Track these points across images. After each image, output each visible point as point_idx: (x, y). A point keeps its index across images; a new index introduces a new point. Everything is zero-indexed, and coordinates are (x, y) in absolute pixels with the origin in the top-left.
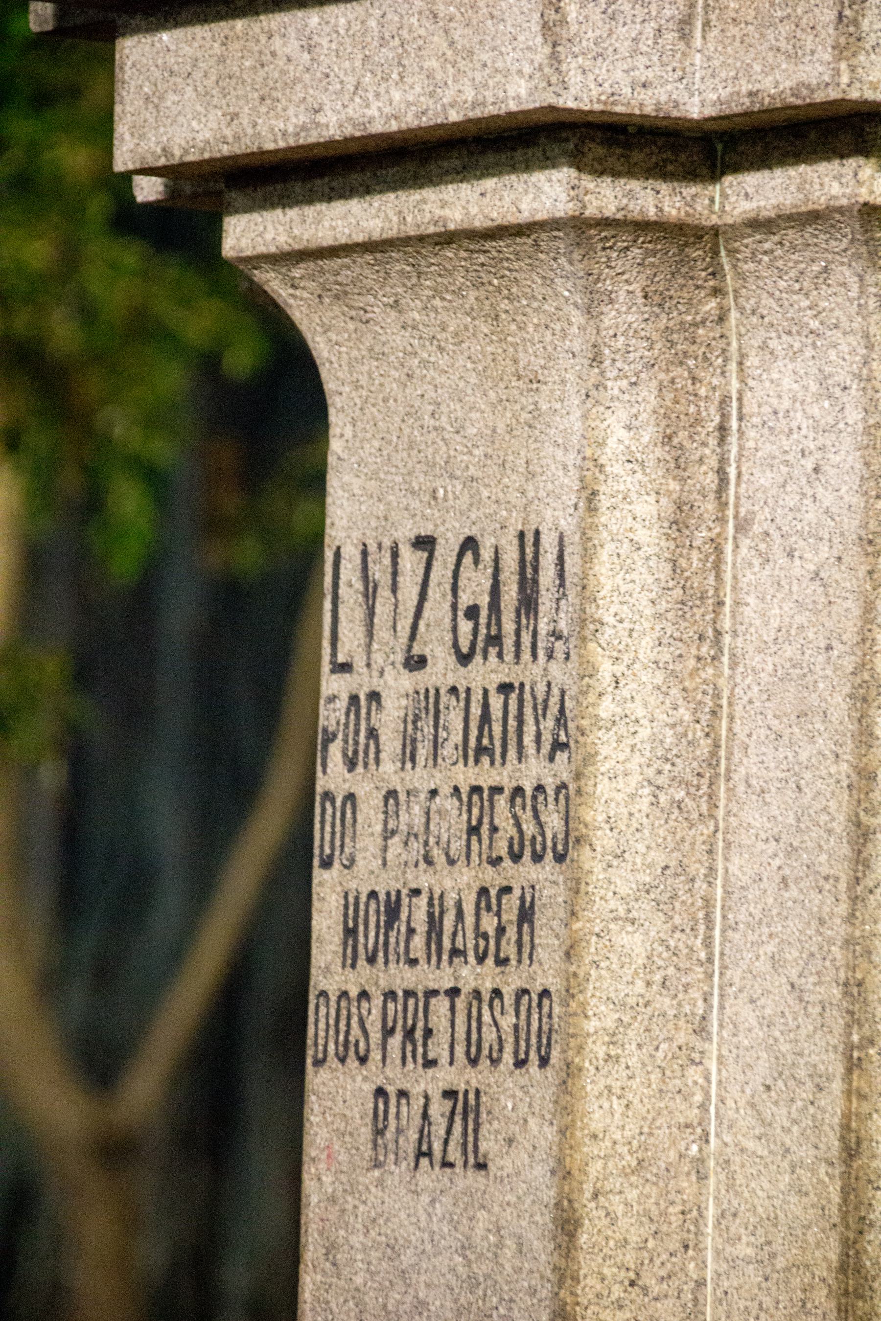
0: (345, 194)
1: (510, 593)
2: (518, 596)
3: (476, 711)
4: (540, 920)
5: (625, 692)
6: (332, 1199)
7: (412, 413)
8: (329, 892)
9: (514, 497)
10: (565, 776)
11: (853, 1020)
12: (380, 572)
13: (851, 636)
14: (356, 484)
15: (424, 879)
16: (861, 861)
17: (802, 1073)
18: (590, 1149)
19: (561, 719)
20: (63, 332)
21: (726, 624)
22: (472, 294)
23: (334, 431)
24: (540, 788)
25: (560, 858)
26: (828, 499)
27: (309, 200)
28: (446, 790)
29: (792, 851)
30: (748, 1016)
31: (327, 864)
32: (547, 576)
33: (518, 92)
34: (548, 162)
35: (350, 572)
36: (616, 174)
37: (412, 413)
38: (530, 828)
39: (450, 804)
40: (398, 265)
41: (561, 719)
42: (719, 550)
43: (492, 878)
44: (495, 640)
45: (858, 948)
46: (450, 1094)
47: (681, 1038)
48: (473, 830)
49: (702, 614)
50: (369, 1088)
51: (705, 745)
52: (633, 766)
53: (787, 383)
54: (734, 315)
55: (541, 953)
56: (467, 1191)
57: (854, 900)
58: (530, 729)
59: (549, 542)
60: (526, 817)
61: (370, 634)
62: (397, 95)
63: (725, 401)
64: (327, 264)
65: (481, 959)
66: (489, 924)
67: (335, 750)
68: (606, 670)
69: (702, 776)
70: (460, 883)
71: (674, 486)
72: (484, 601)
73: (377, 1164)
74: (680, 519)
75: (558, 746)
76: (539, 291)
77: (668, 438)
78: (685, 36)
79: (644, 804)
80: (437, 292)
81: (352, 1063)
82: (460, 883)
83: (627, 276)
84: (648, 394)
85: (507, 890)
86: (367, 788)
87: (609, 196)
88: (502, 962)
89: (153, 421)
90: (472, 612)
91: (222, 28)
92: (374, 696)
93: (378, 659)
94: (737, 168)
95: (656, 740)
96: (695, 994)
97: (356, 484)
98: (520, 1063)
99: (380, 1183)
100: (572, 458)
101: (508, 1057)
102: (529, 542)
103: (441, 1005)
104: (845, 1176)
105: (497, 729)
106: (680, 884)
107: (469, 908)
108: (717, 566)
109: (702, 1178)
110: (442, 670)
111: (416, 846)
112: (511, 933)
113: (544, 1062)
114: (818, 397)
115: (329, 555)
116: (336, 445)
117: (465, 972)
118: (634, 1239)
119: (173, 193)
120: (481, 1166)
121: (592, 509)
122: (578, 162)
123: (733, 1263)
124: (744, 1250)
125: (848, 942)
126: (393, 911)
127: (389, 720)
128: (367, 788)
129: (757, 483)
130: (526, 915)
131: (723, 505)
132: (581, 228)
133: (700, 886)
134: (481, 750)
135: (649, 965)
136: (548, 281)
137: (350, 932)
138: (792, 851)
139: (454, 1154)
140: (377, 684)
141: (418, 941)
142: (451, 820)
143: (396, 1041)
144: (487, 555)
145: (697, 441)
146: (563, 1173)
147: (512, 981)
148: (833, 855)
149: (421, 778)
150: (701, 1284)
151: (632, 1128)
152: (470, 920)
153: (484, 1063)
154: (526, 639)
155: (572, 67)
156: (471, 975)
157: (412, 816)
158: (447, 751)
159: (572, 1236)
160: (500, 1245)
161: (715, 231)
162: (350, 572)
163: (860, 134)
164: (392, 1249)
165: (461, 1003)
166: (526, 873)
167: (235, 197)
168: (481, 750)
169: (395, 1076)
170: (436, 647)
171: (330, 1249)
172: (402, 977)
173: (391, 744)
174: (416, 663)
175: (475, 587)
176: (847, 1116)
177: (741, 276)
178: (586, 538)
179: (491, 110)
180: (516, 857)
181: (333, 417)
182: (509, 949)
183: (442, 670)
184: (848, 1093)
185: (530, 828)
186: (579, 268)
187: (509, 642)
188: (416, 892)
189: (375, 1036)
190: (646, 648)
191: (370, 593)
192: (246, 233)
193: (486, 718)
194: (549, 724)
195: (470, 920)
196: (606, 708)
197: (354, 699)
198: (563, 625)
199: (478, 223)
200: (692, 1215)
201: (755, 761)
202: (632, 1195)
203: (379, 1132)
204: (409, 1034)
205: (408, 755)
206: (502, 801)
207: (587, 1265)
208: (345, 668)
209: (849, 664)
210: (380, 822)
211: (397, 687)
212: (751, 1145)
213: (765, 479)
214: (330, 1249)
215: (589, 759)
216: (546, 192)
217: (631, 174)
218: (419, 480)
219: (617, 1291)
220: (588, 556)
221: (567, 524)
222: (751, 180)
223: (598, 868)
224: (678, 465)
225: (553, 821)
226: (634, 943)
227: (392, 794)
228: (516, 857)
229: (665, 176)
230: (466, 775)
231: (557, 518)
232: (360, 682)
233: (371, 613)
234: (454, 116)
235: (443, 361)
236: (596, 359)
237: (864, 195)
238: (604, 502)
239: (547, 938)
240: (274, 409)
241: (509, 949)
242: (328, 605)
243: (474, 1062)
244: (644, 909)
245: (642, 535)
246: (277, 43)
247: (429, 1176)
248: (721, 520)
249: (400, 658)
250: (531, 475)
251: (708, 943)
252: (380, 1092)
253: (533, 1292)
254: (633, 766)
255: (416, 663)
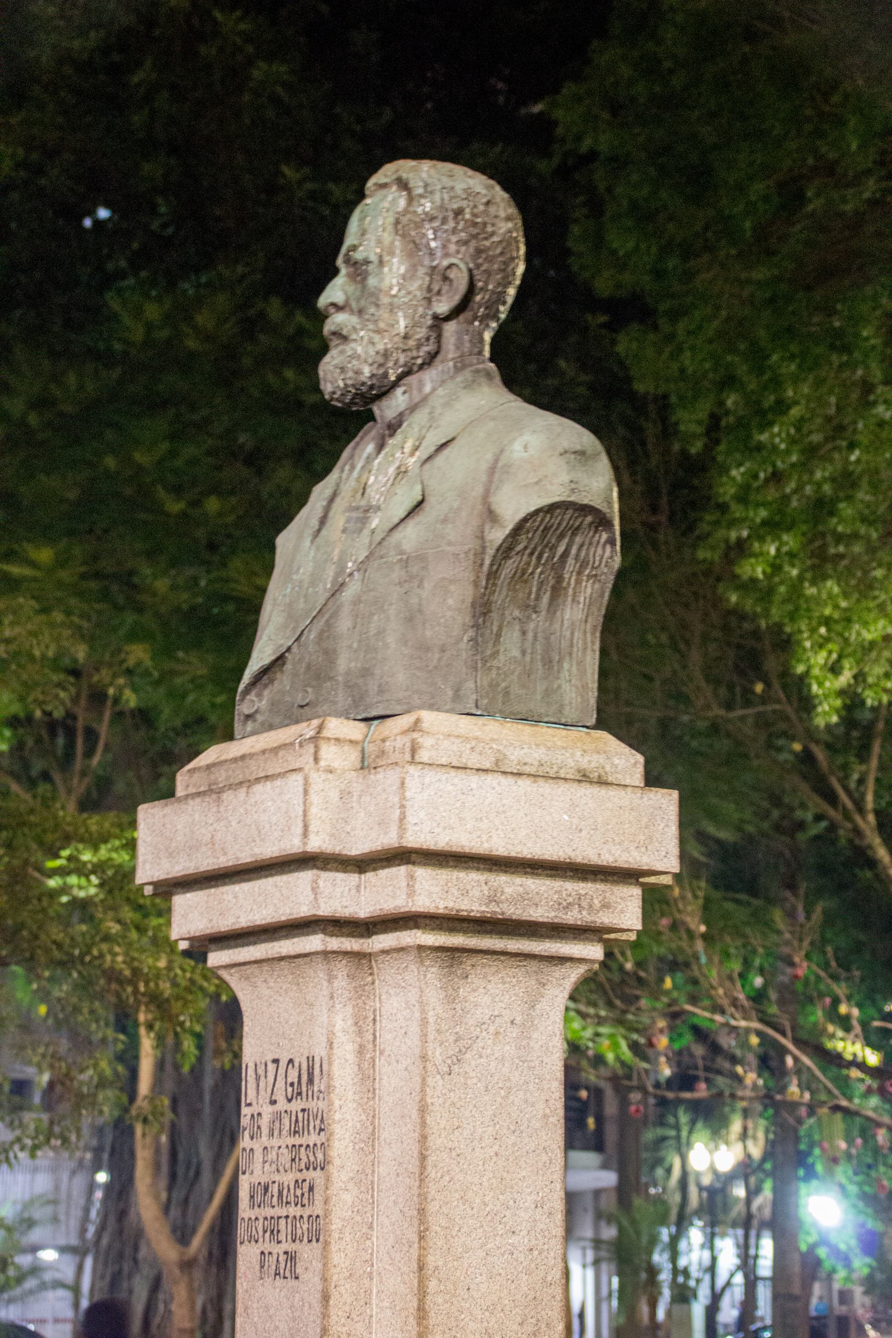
0: (248, 945)
1: (305, 1078)
2: (307, 1078)
3: (294, 1118)
4: (316, 1190)
5: (343, 1110)
6: (247, 1291)
7: (271, 1017)
8: (245, 1183)
9: (306, 1045)
10: (324, 1140)
11: (421, 1222)
12: (261, 1071)
13: (418, 1089)
14: (253, 1042)
15: (277, 1178)
16: (423, 1167)
17: (404, 1241)
18: (333, 1270)
19: (322, 1121)
20: (166, 988)
21: (377, 1086)
22: (291, 977)
23: (245, 1024)
24: (315, 1145)
25: (322, 1169)
26: (409, 1043)
27: (236, 947)
28: (284, 1146)
29: (400, 1164)
30: (386, 1222)
31: (244, 1173)
32: (317, 1071)
33: (304, 910)
34: (314, 933)
35: (251, 1071)
36: (337, 936)
37: (271, 1017)
38: (312, 1159)
39: (285, 1151)
40: (266, 967)
41: (322, 1121)
42: (374, 1061)
43: (299, 1176)
44: (300, 1094)
45: (423, 1197)
46: (286, 1253)
47: (364, 1230)
48: (293, 1160)
49: (369, 1083)
50: (259, 1252)
51: (371, 1128)
52: (346, 1136)
53: (395, 1004)
54: (377, 982)
55: (316, 1202)
56: (292, 1287)
57: (421, 1180)
58: (312, 1124)
59: (317, 1060)
60: (311, 1154)
61: (258, 1093)
62: (264, 912)
63: (375, 1011)
64: (245, 967)
65: (296, 1205)
66: (299, 1192)
67: (246, 1133)
68: (337, 1103)
69: (370, 1138)
70: (288, 1179)
71: (359, 1039)
72: (296, 1080)
73: (262, 1279)
74: (361, 1051)
75: (321, 1130)
76: (312, 975)
77: (356, 1023)
78: (358, 891)
79: (350, 1149)
80: (279, 976)
81: (253, 1243)
82: (288, 1179)
83: (341, 969)
84: (349, 1009)
85: (304, 1180)
86: (257, 1146)
87: (335, 943)
88: (303, 1206)
89: (197, 1018)
90: (292, 1084)
91: (207, 891)
92: (259, 1114)
93: (261, 1101)
94: (376, 933)
95: (354, 1127)
96: (369, 1215)
97: (253, 1042)
98: (310, 1241)
99: (263, 1285)
100: (324, 1031)
101: (305, 1239)
102: (310, 1060)
103: (283, 1222)
104: (419, 1277)
105: (301, 1124)
106: (363, 1176)
107: (292, 1187)
108: (374, 1065)
109: (371, 1279)
110: (282, 1105)
111: (274, 1166)
112: (306, 1195)
113: (318, 1240)
114: (405, 1009)
115: (244, 1066)
116: (246, 1029)
117: (291, 1210)
118: (349, 1302)
119: (191, 946)
120: (297, 1278)
121: (331, 1048)
122: (324, 932)
123: (382, 1309)
124: (386, 1304)
125: (419, 1195)
126: (266, 1189)
127: (265, 1122)
128: (257, 1146)
129: (386, 1038)
130: (311, 1189)
131: (375, 1046)
132: (326, 954)
133: (370, 1177)
134: (295, 1132)
135: (353, 1206)
136: (315, 972)
137: (252, 1197)
138: (400, 1164)
139: (288, 1274)
140: (260, 1110)
141: (275, 1199)
142: (286, 1156)
143: (268, 1234)
144: (296, 1064)
145: (366, 1024)
146: (324, 1279)
147: (306, 1212)
148: (413, 1165)
149: (275, 1142)
150: (371, 1316)
151: (347, 1263)
152: (292, 1191)
153: (298, 1241)
154: (310, 1093)
155: (321, 901)
156: (293, 1211)
157: (272, 1156)
158: (284, 1132)
159: (327, 1301)
160: (303, 1305)
161: (370, 954)
162: (251, 1071)
163: (416, 922)
164: (267, 1308)
165: (289, 1221)
166: (311, 1175)
167: (213, 947)
168: (295, 1132)
169: (267, 1247)
170: (280, 1097)
171: (246, 1308)
172: (269, 1212)
173: (265, 1131)
174: (273, 1102)
175: (293, 1076)
176: (419, 1256)
177: (379, 969)
178: (329, 1058)
179: (295, 916)
180: (308, 1169)
181: (245, 1019)
182: (305, 1201)
183: (282, 1105)
184: (420, 1248)
185: (312, 1159)
186: (326, 967)
187: (304, 1094)
188: (274, 1182)
189: (261, 1233)
190: (350, 1095)
191: (258, 1079)
192: (216, 958)
193: (297, 1121)
194: (318, 1122)
195: (292, 1191)
196: (337, 1116)
197: (253, 1116)
198: (322, 1088)
199: (292, 953)
200: (368, 1292)
201: (386, 1134)
202: (348, 1286)
203: (262, 1267)
204: (272, 1232)
205: (271, 1134)
206: (303, 1149)
207: (332, 1311)
208: (250, 1105)
209: (418, 1099)
210: (260, 1159)
211: (267, 1111)
212: (387, 1267)
213: (389, 1036)
214: (246, 1308)
215: (331, 1134)
216: (314, 942)
217: (342, 936)
218: (274, 1040)
219: (343, 1320)
220: (330, 1064)
221: (324, 1053)
222: (381, 937)
223: (335, 1172)
224: (360, 1032)
225: (320, 1156)
226: (348, 1198)
227: (265, 1148)
228: (308, 1169)
229: (353, 936)
230: (291, 1141)
231: (320, 1051)
232: (255, 1109)
233: (258, 1086)
234: (283, 918)
235: (281, 999)
236: (332, 998)
237: (418, 942)
238: (335, 1046)
239: (318, 1197)
240: (230, 1016)
241: (305, 1201)
242: (243, 1083)
243: (294, 1241)
244: (351, 1186)
245: (348, 1057)
246: (225, 896)
247: (279, 1282)
248: (375, 1051)
249: (268, 1101)
250: (311, 1037)
251: (372, 1196)
252: (262, 1253)
253: (314, 1322)
254: (346, 1136)
255: (273, 1102)
